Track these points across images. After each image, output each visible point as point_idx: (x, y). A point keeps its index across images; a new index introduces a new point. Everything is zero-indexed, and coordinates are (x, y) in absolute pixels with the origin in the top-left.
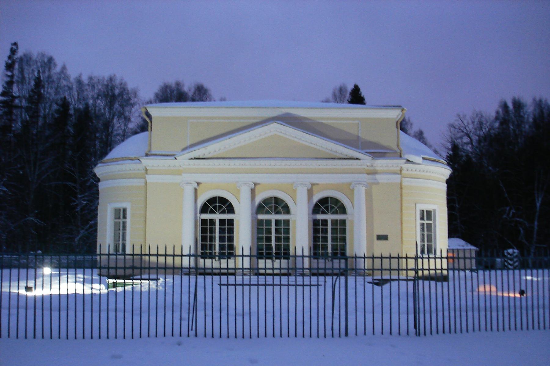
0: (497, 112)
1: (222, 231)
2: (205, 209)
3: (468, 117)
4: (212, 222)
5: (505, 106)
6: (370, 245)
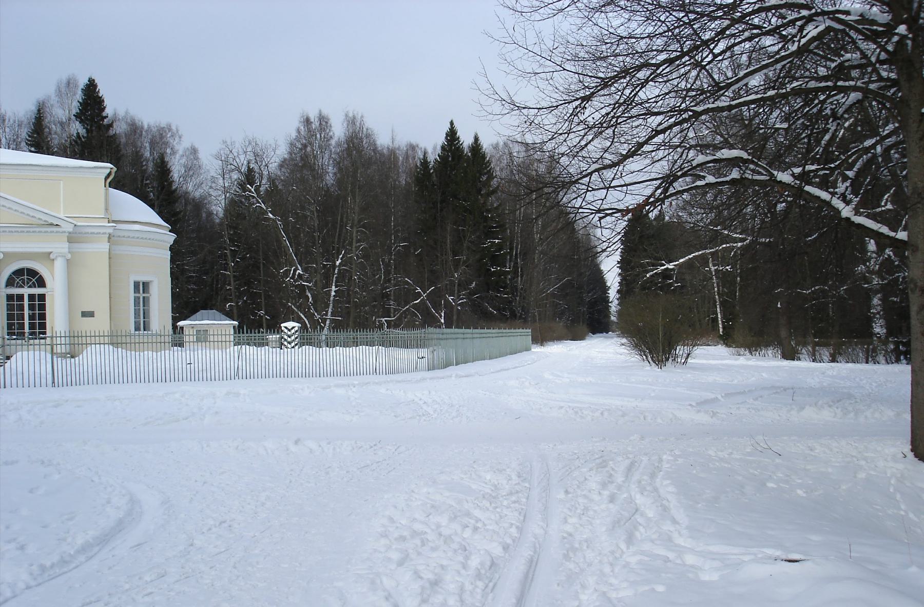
0: (298, 131)
1: (32, 307)
2: (10, 283)
3: (237, 145)
4: (21, 297)
5: (307, 121)
6: (71, 320)
